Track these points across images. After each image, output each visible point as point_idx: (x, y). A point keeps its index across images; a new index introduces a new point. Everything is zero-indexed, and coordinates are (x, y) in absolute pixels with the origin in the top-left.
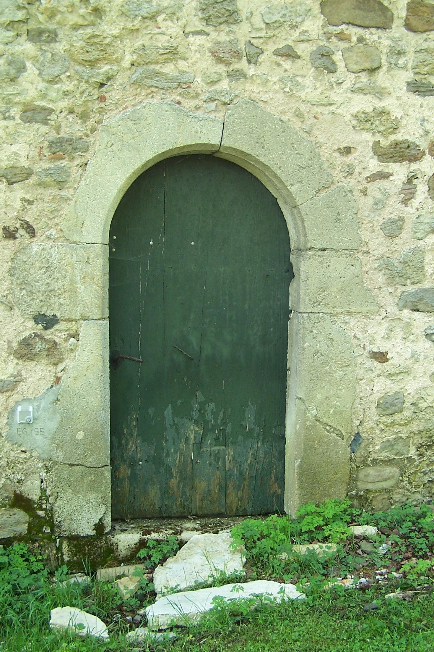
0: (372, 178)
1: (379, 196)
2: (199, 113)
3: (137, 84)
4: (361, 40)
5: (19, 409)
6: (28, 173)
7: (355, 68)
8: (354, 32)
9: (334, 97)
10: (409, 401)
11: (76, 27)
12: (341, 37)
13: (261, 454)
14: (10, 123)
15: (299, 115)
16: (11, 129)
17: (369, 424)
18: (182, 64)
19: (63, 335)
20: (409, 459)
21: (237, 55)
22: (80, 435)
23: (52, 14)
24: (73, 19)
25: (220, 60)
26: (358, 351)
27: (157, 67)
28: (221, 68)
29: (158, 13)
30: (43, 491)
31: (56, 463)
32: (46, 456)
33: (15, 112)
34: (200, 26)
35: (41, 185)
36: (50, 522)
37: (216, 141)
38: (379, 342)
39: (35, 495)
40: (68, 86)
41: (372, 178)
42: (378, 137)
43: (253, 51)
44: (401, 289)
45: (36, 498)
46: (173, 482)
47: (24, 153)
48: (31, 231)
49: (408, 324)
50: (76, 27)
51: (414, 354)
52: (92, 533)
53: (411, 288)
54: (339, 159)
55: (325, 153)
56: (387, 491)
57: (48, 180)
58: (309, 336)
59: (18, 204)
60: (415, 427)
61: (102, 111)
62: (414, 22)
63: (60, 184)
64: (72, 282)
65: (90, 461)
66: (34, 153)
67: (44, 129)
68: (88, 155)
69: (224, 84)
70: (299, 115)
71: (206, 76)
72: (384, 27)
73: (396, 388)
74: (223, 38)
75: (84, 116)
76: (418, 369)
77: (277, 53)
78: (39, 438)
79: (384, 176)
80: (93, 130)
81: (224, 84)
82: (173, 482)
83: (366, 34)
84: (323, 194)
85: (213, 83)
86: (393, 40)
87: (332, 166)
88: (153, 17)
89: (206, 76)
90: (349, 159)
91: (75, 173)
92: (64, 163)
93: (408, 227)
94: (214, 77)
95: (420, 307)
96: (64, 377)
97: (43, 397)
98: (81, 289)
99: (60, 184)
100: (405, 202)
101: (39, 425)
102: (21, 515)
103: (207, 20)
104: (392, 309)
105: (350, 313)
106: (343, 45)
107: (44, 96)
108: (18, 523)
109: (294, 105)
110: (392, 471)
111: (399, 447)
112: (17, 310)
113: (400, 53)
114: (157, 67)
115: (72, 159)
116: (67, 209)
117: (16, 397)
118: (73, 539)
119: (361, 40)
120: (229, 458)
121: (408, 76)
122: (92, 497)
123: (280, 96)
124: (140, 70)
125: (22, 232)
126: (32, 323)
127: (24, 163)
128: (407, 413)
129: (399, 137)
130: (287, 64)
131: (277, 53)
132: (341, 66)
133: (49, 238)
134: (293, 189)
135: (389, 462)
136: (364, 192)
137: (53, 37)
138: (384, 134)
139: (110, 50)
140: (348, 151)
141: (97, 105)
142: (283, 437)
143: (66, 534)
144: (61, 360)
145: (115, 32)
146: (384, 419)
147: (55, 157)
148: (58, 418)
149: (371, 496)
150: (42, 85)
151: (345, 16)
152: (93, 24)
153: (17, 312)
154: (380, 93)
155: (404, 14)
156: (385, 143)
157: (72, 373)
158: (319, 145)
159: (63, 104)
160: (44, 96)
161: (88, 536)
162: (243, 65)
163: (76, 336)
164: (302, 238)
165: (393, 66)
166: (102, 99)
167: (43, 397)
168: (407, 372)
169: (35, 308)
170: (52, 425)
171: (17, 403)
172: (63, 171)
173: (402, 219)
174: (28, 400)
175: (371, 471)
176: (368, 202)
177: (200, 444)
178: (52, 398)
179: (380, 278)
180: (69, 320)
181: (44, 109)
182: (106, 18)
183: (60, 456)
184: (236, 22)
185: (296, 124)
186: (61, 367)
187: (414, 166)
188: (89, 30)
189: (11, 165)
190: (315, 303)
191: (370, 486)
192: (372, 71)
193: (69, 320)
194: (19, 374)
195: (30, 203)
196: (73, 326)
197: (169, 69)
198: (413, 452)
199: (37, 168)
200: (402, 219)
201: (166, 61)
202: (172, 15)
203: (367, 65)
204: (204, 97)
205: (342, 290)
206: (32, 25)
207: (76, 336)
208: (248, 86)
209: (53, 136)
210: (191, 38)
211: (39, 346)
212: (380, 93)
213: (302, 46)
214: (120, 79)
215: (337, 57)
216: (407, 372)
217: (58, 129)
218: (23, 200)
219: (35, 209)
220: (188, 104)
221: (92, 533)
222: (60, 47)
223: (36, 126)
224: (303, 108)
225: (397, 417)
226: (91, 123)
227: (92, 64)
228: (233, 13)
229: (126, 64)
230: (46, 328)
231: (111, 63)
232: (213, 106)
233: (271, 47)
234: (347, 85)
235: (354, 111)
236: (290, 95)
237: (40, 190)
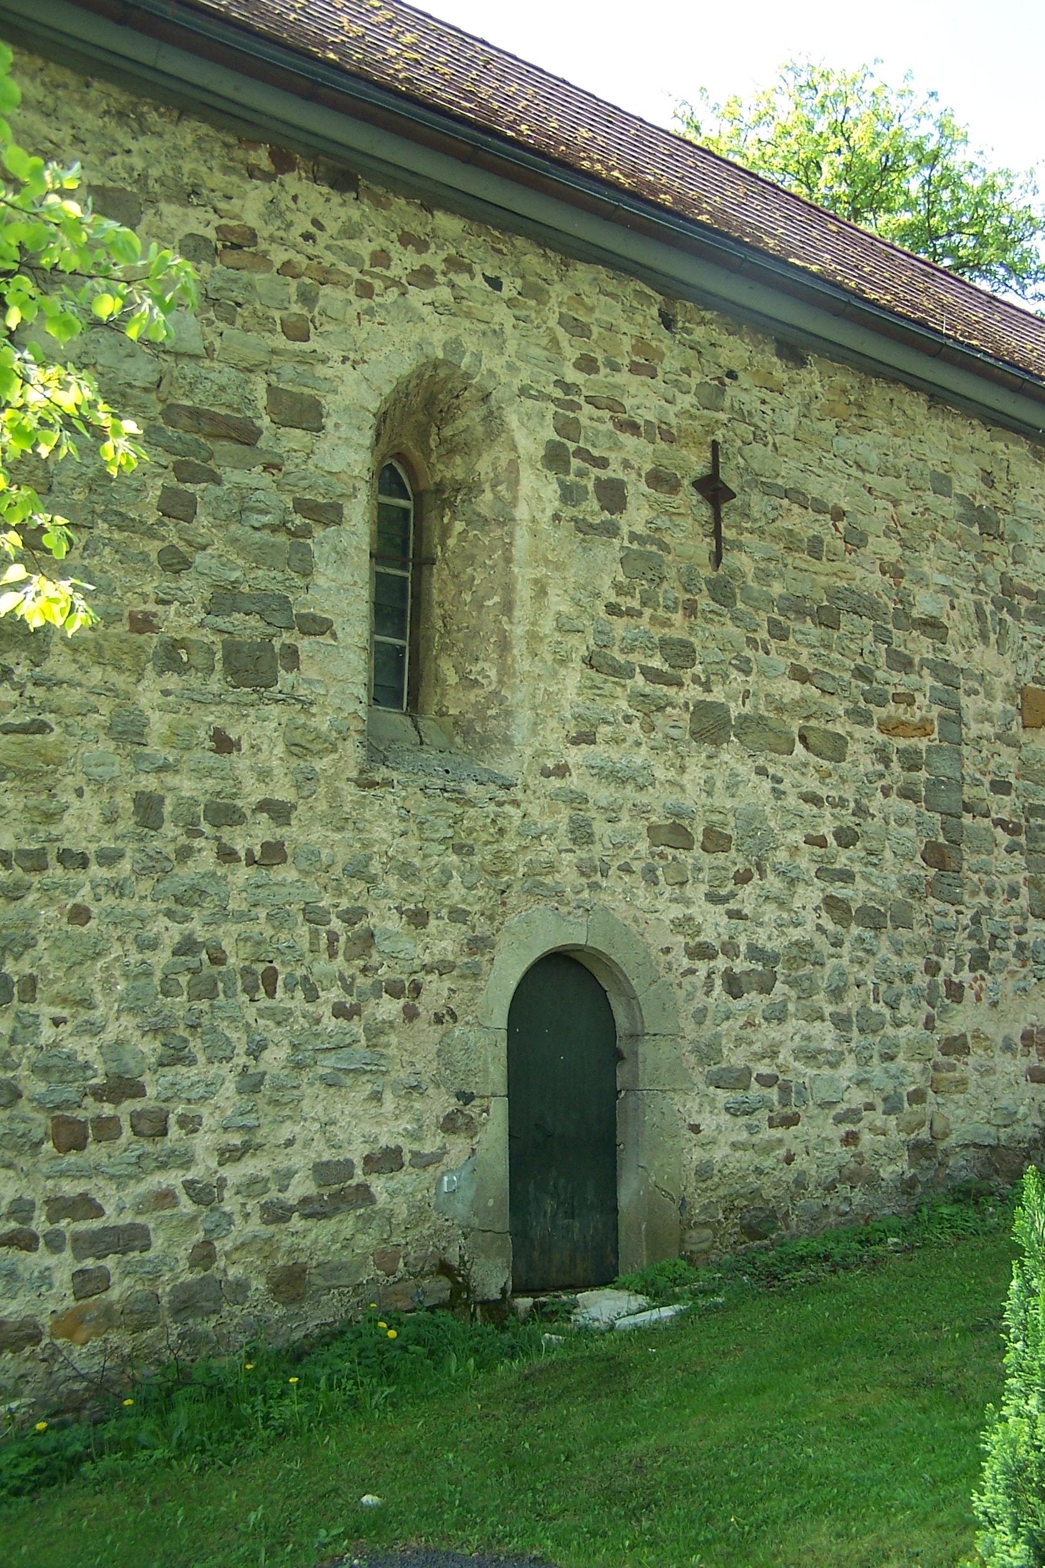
0: (684, 974)
1: (690, 988)
2: (571, 918)
3: (528, 892)
4: (674, 858)
5: (446, 1179)
6: (452, 966)
7: (671, 881)
8: (669, 851)
9: (660, 907)
10: (717, 1168)
11: (487, 843)
12: (662, 856)
13: (600, 1226)
14: (441, 923)
15: (636, 921)
16: (441, 928)
17: (690, 1190)
18: (557, 875)
19: (477, 1110)
20: (719, 1221)
21: (594, 869)
22: (491, 1203)
23: (470, 831)
24: (485, 837)
25: (583, 874)
26: (681, 1123)
27: (541, 878)
28: (584, 881)
29: (542, 833)
30: (462, 1257)
31: (472, 1229)
32: (464, 1223)
33: (444, 912)
34: (570, 846)
35: (463, 977)
36: (468, 1289)
37: (583, 942)
38: (694, 1115)
39: (456, 1263)
40: (481, 892)
41: (684, 974)
42: (688, 939)
43: (606, 867)
44: (707, 1068)
45: (456, 1264)
46: (536, 1254)
47: (450, 949)
48: (454, 1017)
49: (714, 1100)
50: (487, 843)
51: (718, 1126)
52: (499, 1297)
53: (714, 1068)
54: (663, 958)
55: (653, 951)
56: (706, 1252)
57: (467, 972)
58: (648, 1111)
59: (446, 993)
60: (722, 1192)
61: (504, 914)
62: (708, 845)
63: (476, 976)
64: (485, 1062)
65: (498, 1227)
66: (457, 949)
67: (464, 928)
68: (494, 951)
69: (585, 894)
70: (636, 921)
71: (573, 887)
72: (689, 848)
73: (707, 1156)
74: (585, 855)
75: (491, 918)
76: (722, 1139)
77: (619, 868)
78: (460, 1206)
79: (692, 972)
80: (498, 930)
81: (585, 894)
82: (536, 1254)
83: (677, 853)
84: (653, 987)
85: (578, 893)
86: (694, 858)
87: (658, 963)
88: (538, 837)
89: (573, 887)
90: (669, 957)
91: (486, 967)
92: (477, 958)
93: (710, 1015)
94: (579, 888)
95: (722, 1084)
96: (480, 1151)
97: (462, 1168)
98: (492, 1069)
99: (476, 976)
100: (707, 994)
101: (460, 1194)
102: (445, 1282)
103: (574, 841)
104: (702, 1086)
105: (674, 1090)
106: (663, 862)
107: (464, 901)
108: (442, 1290)
109: (632, 912)
110: (707, 1232)
111: (711, 1210)
112: (443, 1089)
113: (700, 870)
114: (541, 878)
115: (483, 955)
116: (480, 999)
117: (442, 1168)
118: (485, 1303)
119: (674, 858)
120: (576, 1230)
121: (704, 888)
122: (499, 1261)
123: (623, 904)
124: (530, 880)
125: (447, 1018)
126: (454, 1100)
127: (451, 958)
128: (716, 1179)
129: (701, 938)
130: (626, 878)
131: (619, 868)
132: (662, 878)
133: (467, 1023)
134: (633, 983)
135: (705, 1224)
136: (680, 985)
137: (471, 852)
138: (693, 937)
139: (509, 863)
140: (667, 951)
141: (500, 910)
142: (615, 1210)
143: (479, 1299)
144: (476, 1134)
145: (513, 848)
146: (701, 1185)
147: (472, 954)
148: (475, 1186)
149: (695, 1256)
150: (464, 891)
151: (663, 839)
152: (497, 841)
153: (443, 1089)
154: (688, 902)
155: (701, 838)
156: (692, 944)
157: (485, 1145)
158: (649, 946)
159: (477, 908)
160: (464, 901)
161: (495, 1301)
162: (598, 878)
163: (487, 1111)
164: (639, 1025)
165: (696, 880)
166: (504, 904)
167: (462, 1168)
168: (713, 1142)
169: (457, 1086)
170: (469, 1193)
171: (443, 1174)
172: (478, 965)
173: (706, 1008)
174: (451, 1170)
175: (693, 1233)
176: (681, 994)
177: (554, 1216)
178: (470, 1168)
179: (693, 1059)
180: (483, 1097)
181: (464, 911)
182: (507, 837)
183: (475, 1222)
184: (592, 843)
185: (634, 928)
186: (476, 1140)
187: (712, 964)
188: (495, 846)
189: (958, 1182)
190: (652, 1081)
191: (694, 1248)
192: (682, 884)
193: (483, 1097)
194: (444, 1147)
195: (454, 991)
196: (485, 1102)
197: (548, 880)
198: (721, 1216)
199: (459, 962)
200: (706, 1008)
201: (548, 873)
202: (551, 837)
203: (680, 879)
204: (574, 904)
205: (668, 1070)
206: (456, 841)
207: (487, 1111)
208: (602, 896)
209: (470, 934)
210: (563, 855)
211: (461, 1121)
212: (688, 902)
213: (637, 862)
214: (516, 887)
215: (659, 872)
216: (713, 1142)
217: (473, 928)
218: (450, 989)
219: (457, 997)
220: (564, 910)
221: (499, 1297)
222: (476, 859)
223: (459, 925)
224: (639, 914)
225: (709, 1182)
226: (496, 923)
227: (497, 874)
228: (591, 835)
229: (520, 875)
230: (466, 1104)
231: (509, 874)
232: (580, 912)
233: (616, 864)
234: (666, 895)
235: (672, 917)
236: (630, 904)
237: (461, 981)
